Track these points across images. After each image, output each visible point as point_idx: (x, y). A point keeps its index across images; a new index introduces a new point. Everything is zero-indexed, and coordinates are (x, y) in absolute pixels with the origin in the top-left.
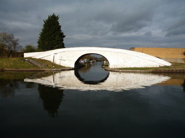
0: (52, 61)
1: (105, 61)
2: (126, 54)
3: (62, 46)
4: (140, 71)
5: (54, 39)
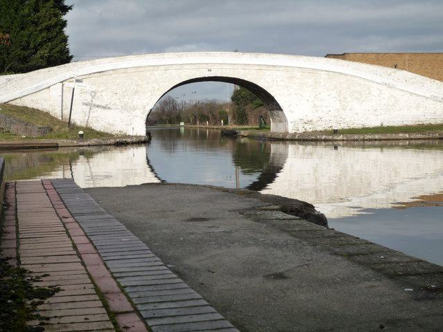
1: (182, 124)
2: (346, 75)
3: (63, 58)
4: (407, 136)
5: (33, 23)
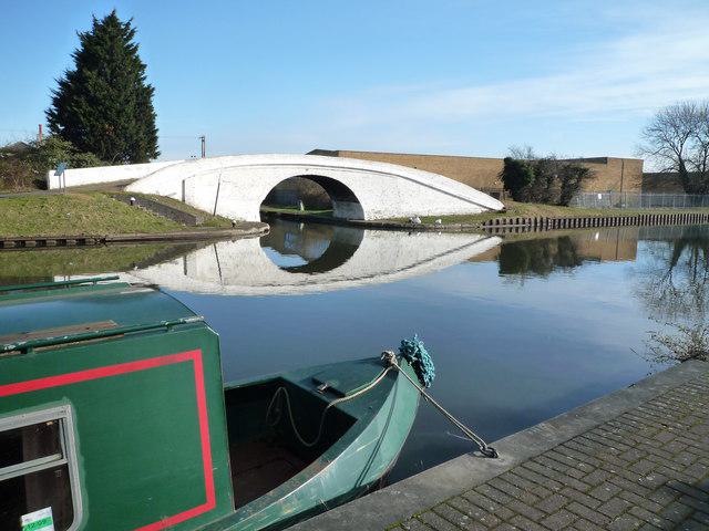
0: (178, 197)
